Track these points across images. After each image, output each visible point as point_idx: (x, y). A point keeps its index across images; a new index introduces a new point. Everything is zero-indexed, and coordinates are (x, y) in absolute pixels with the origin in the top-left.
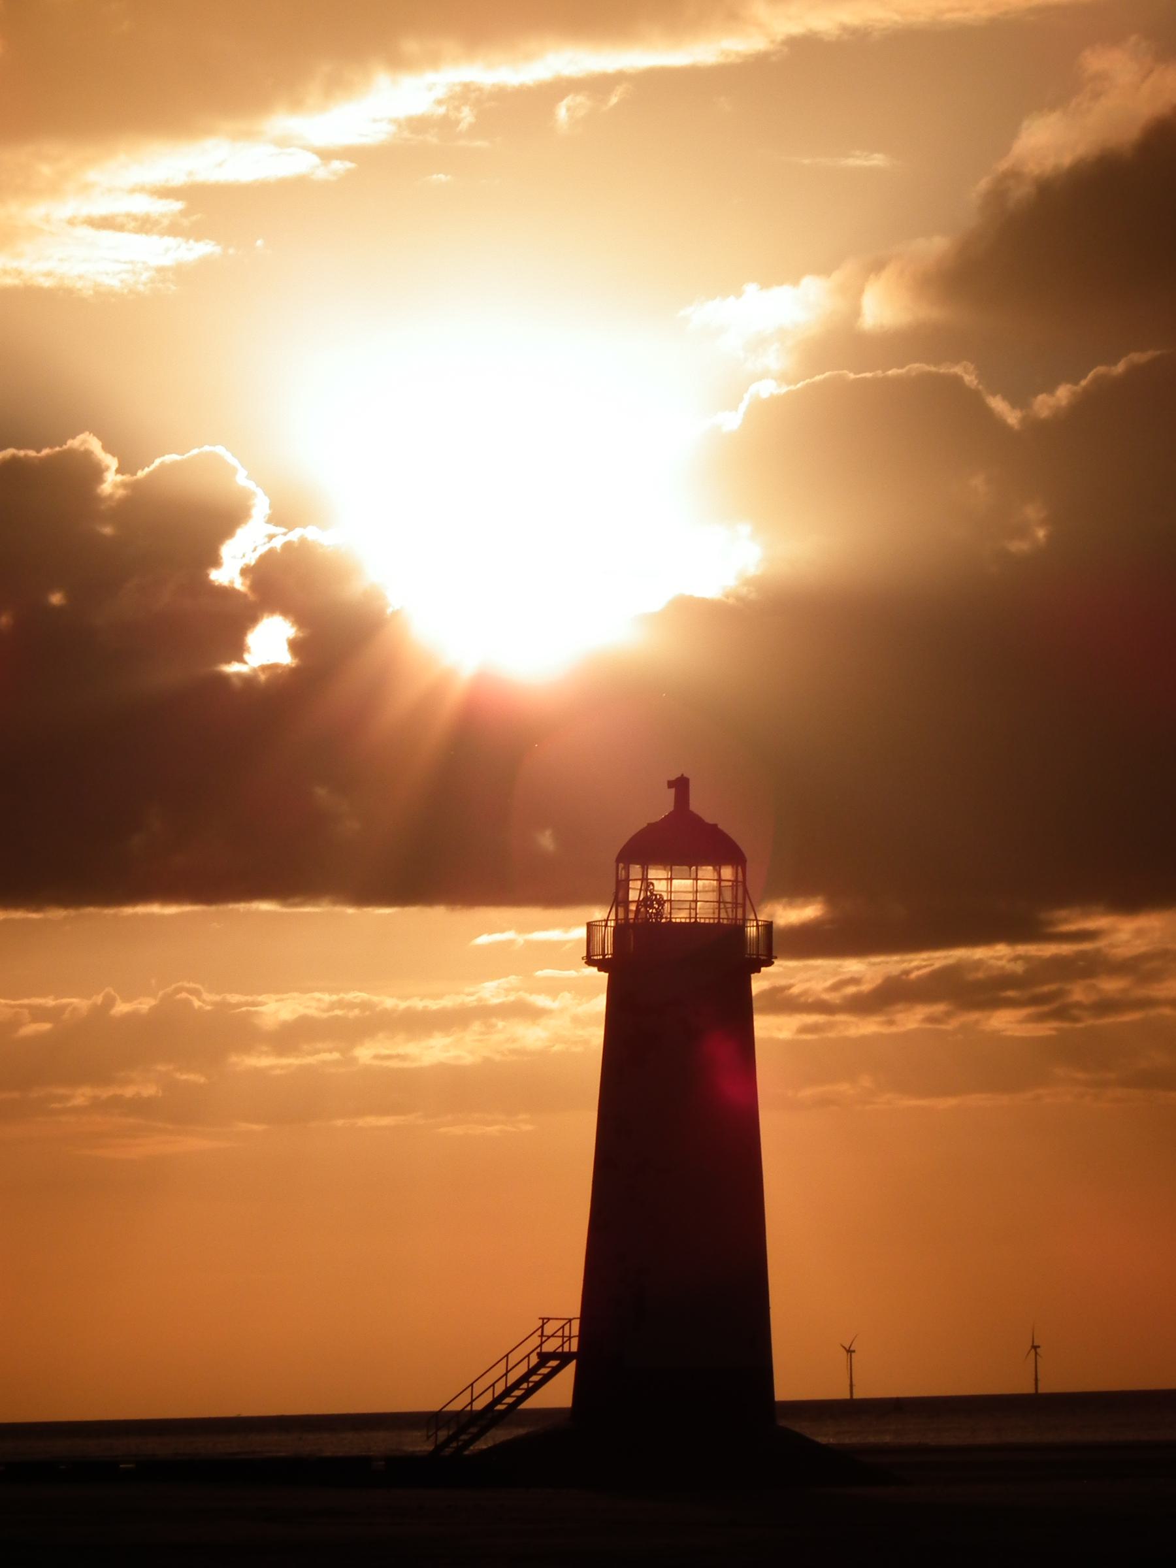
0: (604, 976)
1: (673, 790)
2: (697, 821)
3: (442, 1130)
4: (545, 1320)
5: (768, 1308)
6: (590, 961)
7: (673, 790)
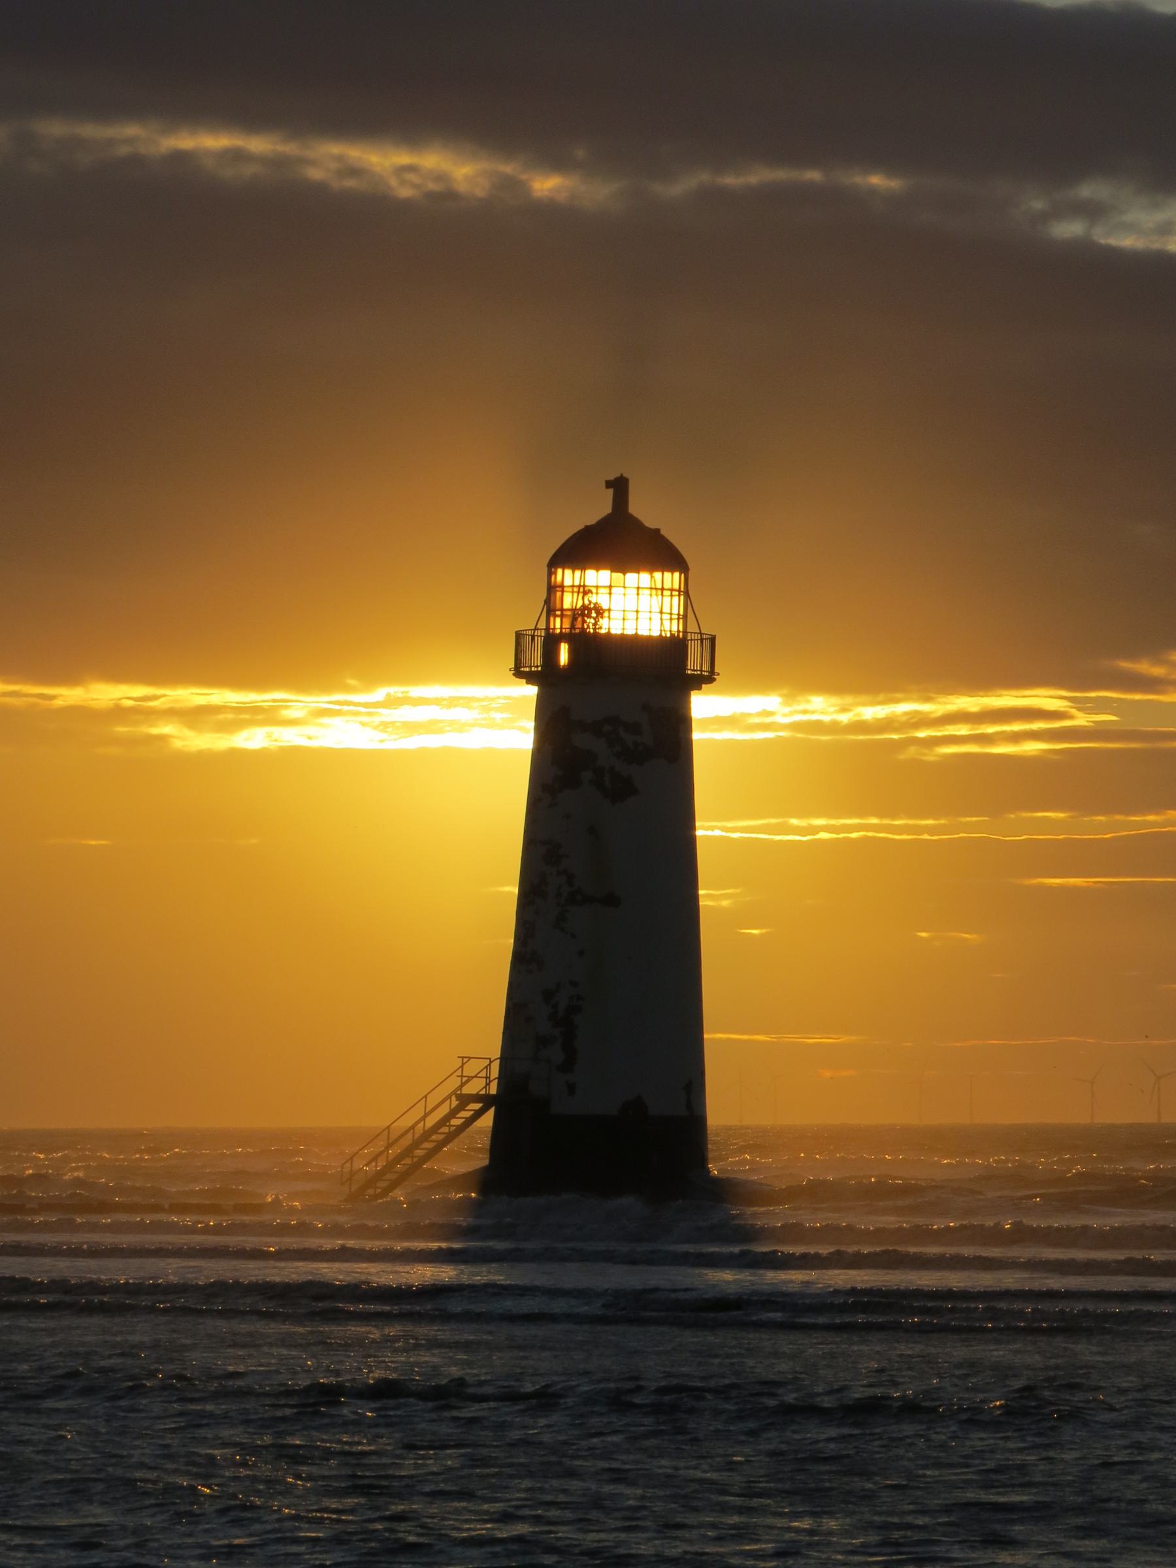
1: (611, 491)
2: (671, 743)
3: (738, 891)
4: (464, 1060)
5: (703, 1073)
6: (518, 673)
7: (611, 491)
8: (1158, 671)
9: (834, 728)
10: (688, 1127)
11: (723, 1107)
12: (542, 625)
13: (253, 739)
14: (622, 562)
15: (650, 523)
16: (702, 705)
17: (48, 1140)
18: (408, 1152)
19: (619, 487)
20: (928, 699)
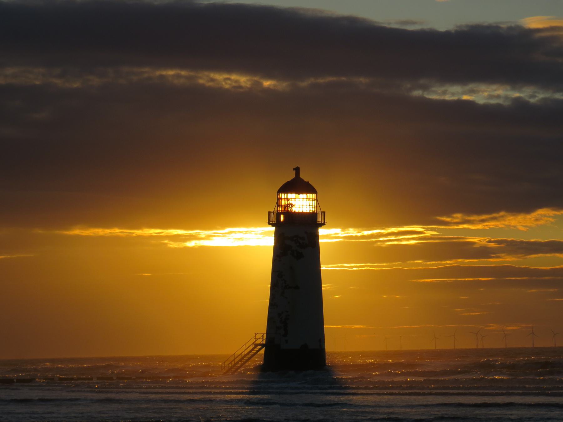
2: (313, 242)
4: (256, 334)
6: (269, 224)
8: (448, 219)
9: (356, 237)
10: (320, 351)
11: (330, 346)
12: (276, 209)
13: (191, 244)
14: (298, 192)
15: (306, 180)
16: (322, 231)
17: (138, 359)
18: (240, 360)
19: (297, 170)
20: (383, 229)
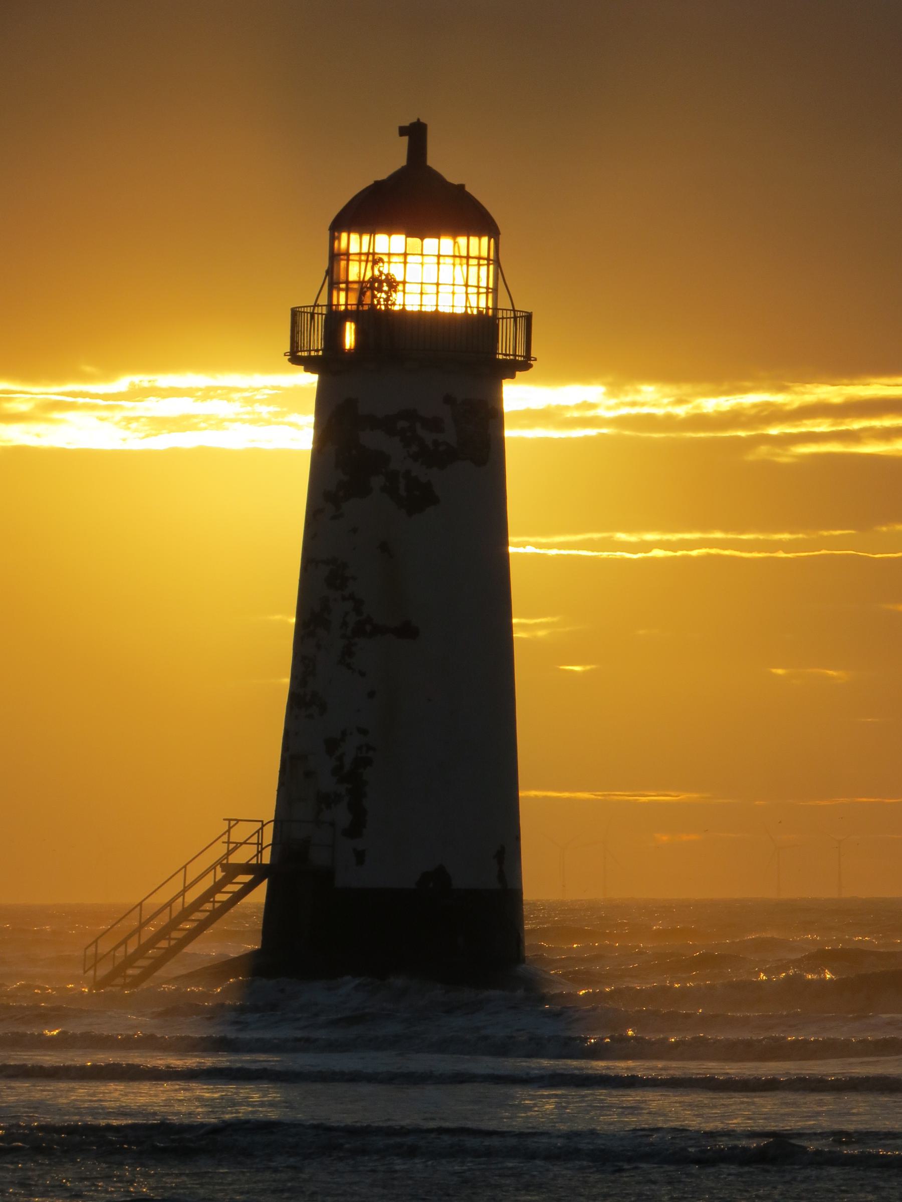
0: (310, 380)
1: (406, 139)
4: (232, 822)
6: (295, 358)
7: (406, 139)
